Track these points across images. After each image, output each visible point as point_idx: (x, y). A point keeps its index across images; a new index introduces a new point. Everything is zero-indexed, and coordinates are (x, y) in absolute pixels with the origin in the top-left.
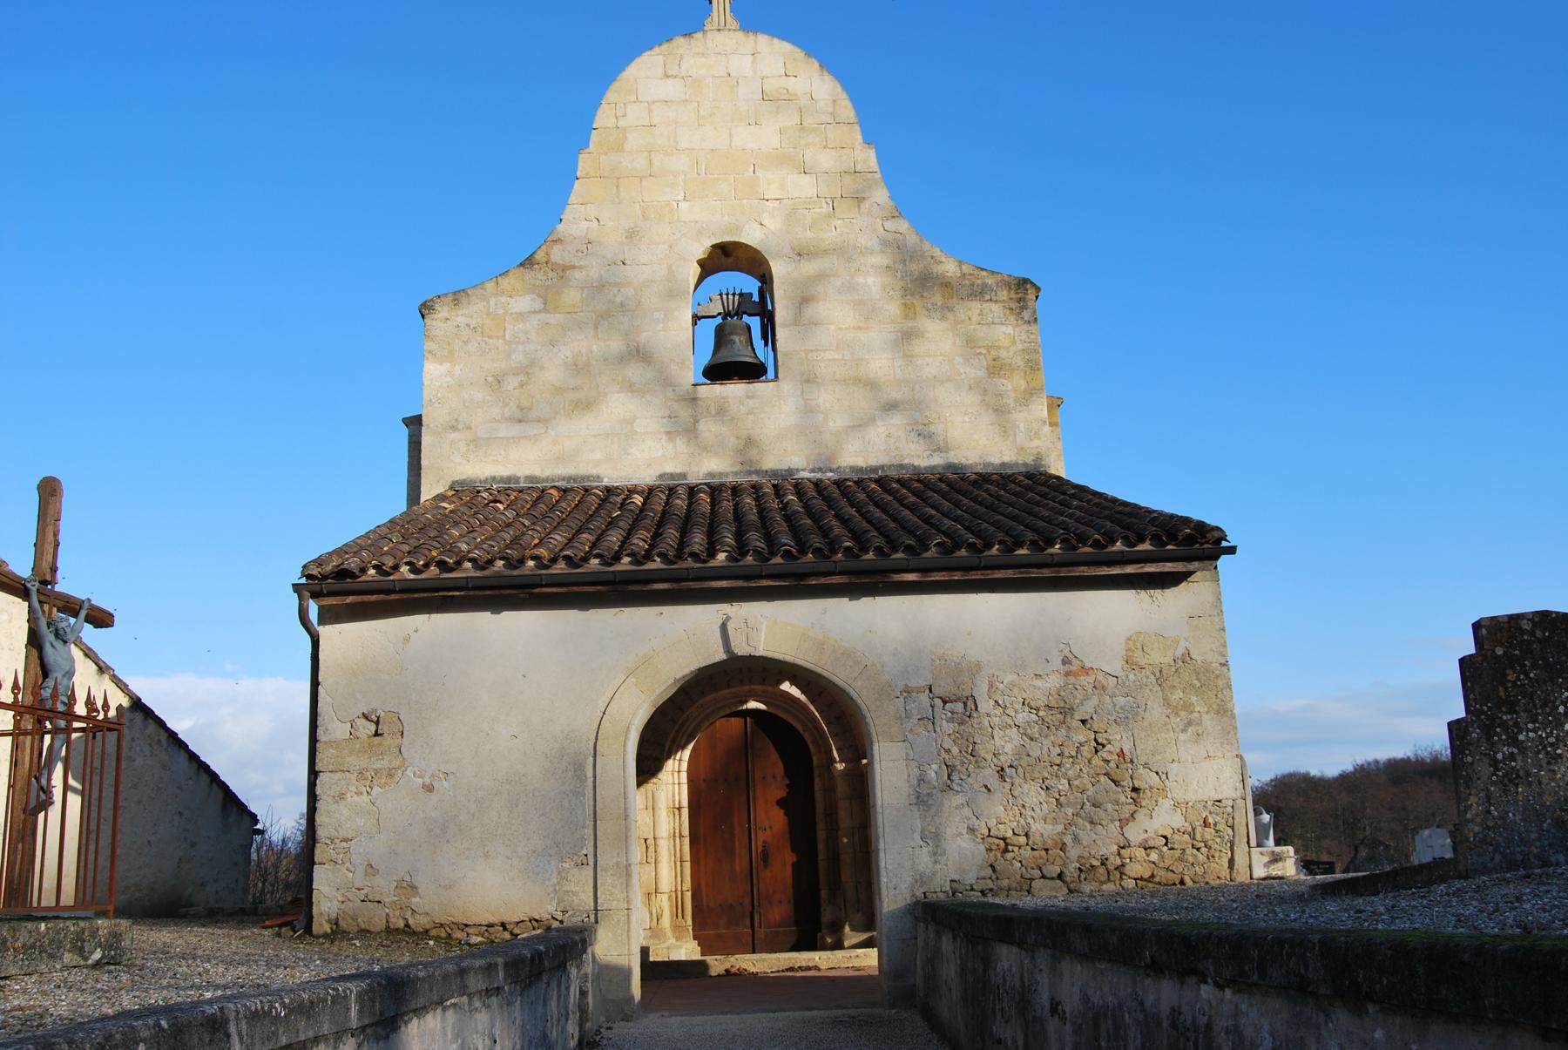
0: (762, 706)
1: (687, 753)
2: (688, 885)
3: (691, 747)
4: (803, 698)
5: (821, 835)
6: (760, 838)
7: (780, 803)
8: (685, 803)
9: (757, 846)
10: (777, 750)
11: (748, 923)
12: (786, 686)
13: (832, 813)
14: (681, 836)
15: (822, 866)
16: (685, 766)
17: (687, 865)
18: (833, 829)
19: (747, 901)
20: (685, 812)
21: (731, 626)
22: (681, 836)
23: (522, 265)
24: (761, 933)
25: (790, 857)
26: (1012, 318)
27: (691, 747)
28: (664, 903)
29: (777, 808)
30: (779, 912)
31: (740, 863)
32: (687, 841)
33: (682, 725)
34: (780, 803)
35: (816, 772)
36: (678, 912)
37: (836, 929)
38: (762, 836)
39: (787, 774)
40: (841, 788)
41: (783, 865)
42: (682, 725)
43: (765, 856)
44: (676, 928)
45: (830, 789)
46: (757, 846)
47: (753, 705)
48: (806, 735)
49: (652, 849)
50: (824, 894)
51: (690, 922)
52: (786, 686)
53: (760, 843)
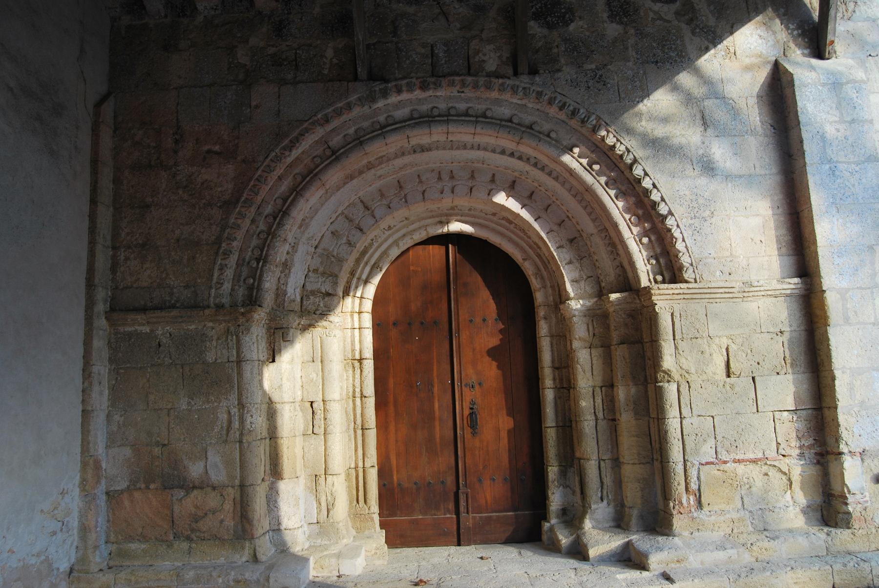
0: (467, 228)
1: (371, 290)
2: (372, 458)
3: (376, 280)
4: (525, 214)
5: (549, 395)
6: (467, 397)
7: (493, 353)
8: (369, 353)
9: (463, 410)
10: (489, 286)
11: (451, 506)
12: (501, 198)
13: (564, 366)
14: (363, 396)
15: (551, 435)
16: (368, 305)
17: (372, 436)
18: (566, 386)
19: (450, 480)
20: (369, 365)
21: (730, 350)
22: (363, 396)
23: (514, 182)
24: (469, 520)
25: (506, 423)
26: (283, 527)
27: (376, 280)
28: (339, 488)
29: (487, 359)
30: (491, 491)
31: (441, 431)
32: (371, 402)
33: (364, 253)
34: (493, 353)
35: (541, 312)
36: (359, 495)
37: (572, 518)
38: (468, 395)
39: (500, 316)
40: (580, 331)
41: (497, 427)
42: (364, 253)
43: (473, 420)
44: (356, 516)
45: (562, 334)
46: (463, 410)
47: (456, 227)
48: (535, 283)
49: (320, 415)
50: (553, 472)
51: (375, 508)
52: (501, 198)
53: (466, 405)
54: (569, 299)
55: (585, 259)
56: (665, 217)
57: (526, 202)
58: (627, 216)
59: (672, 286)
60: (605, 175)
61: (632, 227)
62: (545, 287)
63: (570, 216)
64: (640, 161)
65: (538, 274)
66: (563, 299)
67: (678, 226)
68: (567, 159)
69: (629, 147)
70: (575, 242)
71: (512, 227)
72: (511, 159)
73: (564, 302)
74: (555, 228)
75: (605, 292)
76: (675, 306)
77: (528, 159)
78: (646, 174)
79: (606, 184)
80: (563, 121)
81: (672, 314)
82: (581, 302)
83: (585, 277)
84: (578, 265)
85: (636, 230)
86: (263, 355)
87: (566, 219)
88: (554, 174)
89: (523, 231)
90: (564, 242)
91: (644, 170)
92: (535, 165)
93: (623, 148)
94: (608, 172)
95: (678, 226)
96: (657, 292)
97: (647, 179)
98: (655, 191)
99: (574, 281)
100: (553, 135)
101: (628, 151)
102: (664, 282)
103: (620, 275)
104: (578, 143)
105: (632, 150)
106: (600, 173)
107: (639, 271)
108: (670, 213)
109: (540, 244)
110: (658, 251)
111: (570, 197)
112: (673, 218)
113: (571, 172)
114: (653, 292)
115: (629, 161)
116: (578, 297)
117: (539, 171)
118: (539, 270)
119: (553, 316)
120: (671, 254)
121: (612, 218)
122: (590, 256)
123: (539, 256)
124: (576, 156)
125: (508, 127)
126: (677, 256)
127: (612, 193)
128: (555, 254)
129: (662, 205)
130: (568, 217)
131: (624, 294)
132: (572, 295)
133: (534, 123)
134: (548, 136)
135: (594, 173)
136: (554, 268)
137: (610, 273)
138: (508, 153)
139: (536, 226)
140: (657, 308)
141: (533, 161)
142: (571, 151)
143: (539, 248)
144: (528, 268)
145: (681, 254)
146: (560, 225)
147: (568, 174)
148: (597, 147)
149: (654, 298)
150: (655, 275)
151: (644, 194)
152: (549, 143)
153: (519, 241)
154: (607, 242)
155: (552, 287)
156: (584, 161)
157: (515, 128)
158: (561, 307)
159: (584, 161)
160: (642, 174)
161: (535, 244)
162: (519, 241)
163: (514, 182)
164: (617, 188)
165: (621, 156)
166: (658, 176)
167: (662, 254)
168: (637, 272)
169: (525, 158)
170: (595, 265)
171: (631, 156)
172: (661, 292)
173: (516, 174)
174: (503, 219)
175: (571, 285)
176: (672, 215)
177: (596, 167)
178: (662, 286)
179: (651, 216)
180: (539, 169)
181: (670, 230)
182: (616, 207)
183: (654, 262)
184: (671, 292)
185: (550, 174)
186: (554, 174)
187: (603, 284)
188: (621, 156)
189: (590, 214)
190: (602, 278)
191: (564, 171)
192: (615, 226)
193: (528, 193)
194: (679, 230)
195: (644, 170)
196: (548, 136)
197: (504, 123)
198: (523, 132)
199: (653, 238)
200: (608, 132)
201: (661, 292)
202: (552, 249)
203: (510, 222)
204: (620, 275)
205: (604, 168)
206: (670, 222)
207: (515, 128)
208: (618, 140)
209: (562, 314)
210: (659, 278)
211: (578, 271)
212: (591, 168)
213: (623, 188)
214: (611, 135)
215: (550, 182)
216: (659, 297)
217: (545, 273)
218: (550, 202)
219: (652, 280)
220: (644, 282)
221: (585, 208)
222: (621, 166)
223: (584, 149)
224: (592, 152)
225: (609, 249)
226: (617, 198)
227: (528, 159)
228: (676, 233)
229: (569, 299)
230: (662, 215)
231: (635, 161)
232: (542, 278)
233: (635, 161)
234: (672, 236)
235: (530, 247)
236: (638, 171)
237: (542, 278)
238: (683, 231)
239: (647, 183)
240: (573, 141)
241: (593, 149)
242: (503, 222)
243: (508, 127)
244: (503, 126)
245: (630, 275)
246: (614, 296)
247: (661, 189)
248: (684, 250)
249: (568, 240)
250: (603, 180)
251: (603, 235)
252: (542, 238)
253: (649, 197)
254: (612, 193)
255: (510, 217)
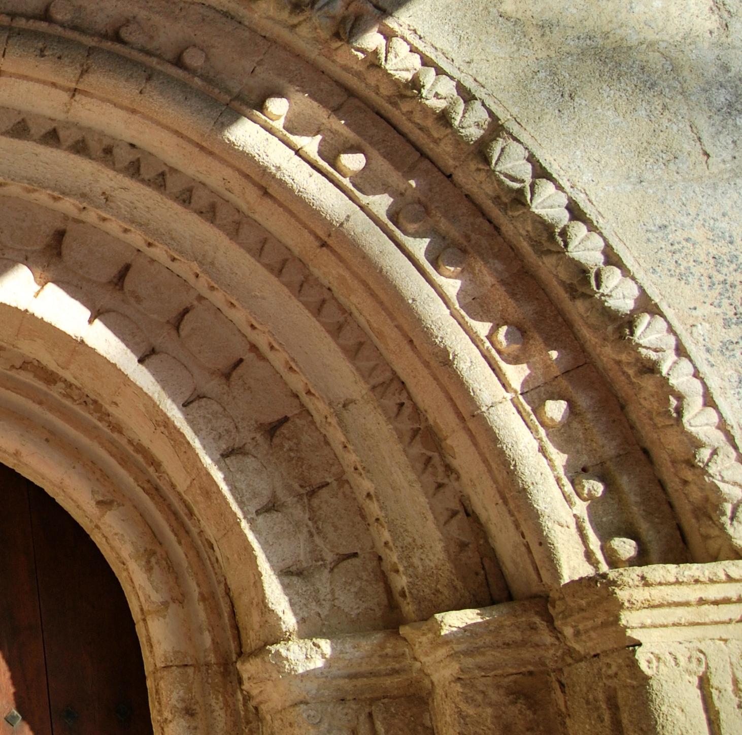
4: (102, 339)
23: (60, 235)
48: (140, 585)
54: (280, 637)
55: (324, 493)
56: (628, 323)
57: (107, 299)
58: (483, 328)
59: (670, 571)
60: (385, 188)
61: (503, 365)
62: (181, 599)
63: (262, 341)
64: (515, 129)
65: (154, 553)
66: (251, 640)
67: (681, 351)
68: (245, 134)
69: (469, 83)
70: (278, 437)
71: (55, 392)
72: (48, 153)
73: (261, 650)
74: (212, 386)
75: (408, 608)
76: (709, 648)
77: (108, 151)
78: (541, 173)
79: (394, 215)
80: (226, 14)
81: (704, 683)
82: (326, 645)
83: (330, 557)
84: (299, 513)
85: (517, 374)
86: (583, 581)
87: (249, 357)
88: (201, 199)
89: (96, 406)
90: (245, 436)
91: (531, 159)
92: (134, 169)
93: (447, 87)
94: (395, 178)
95: (681, 351)
96: (641, 594)
97: (547, 189)
98: (579, 230)
99: (289, 574)
100: (194, 59)
101: (467, 96)
102: (642, 558)
103: (463, 546)
104: (282, 82)
105: (479, 93)
106: (366, 182)
107: (548, 524)
108: (646, 305)
109: (161, 450)
110: (609, 448)
111: (263, 272)
112: (660, 323)
113: (265, 183)
114: (622, 594)
115: (474, 133)
116: (310, 630)
117: (147, 191)
118: (155, 536)
119: (217, 704)
120: (662, 457)
121: (427, 334)
122: (342, 481)
123: (155, 491)
124: (279, 125)
125: (36, 35)
126: (690, 463)
127: (420, 246)
128: (218, 476)
129: (613, 278)
130: (254, 348)
131: (494, 614)
132: (289, 622)
133: (127, 22)
134: (178, 62)
135: (346, 182)
136: (211, 533)
137: (422, 541)
138: (37, 130)
139: (143, 377)
140: (642, 656)
141: (124, 156)
142: (261, 107)
143: (155, 463)
144: (115, 539)
145: (705, 454)
146: (227, 376)
147: (252, 194)
148: (350, 92)
149: (626, 618)
150: (605, 536)
151: (536, 245)
152: (184, 86)
153: (84, 440)
154: (407, 426)
155: (208, 598)
156: (311, 145)
157: (60, 40)
158: (248, 669)
159: (311, 145)
160: (526, 171)
161: (141, 449)
162: (84, 440)
163: (60, 235)
164: (432, 232)
165: (444, 117)
166: (585, 178)
167: (622, 458)
168: (538, 529)
169: (95, 147)
170: (362, 513)
171: (479, 114)
172: (657, 594)
173: (68, 205)
174: (26, 365)
175: (286, 587)
176: (655, 311)
177: (354, 162)
178: (658, 572)
179: (568, 324)
180: (148, 183)
181: (650, 368)
182: (438, 299)
183: (598, 488)
184: (692, 593)
185: (186, 198)
186: (201, 199)
187: (401, 582)
188: (444, 117)
189: (336, 331)
190: (393, 557)
191: (236, 182)
192: (442, 362)
193: (112, 272)
194: (685, 364)
195: (531, 159)
196: (178, 62)
197: (22, 23)
198: (90, 51)
199: (583, 402)
200: (389, 36)
201: (657, 594)
202: (207, 460)
203: (50, 378)
204: (463, 546)
205: (382, 165)
206: (649, 335)
207: (60, 40)
208: (426, 62)
209: (247, 698)
210: (626, 547)
211: (303, 536)
212: (333, 165)
213: (454, 233)
214: (399, 46)
215: (188, 225)
216: (647, 616)
217: (179, 552)
218: (188, 299)
219: (599, 556)
220: (572, 565)
221: (318, 310)
222: (444, 151)
223: (303, 101)
224: (336, 110)
225: (417, 449)
226: (435, 264)
227: (108, 151)
228: (680, 377)
229: (280, 637)
230: (610, 315)
231: (496, 129)
232: (171, 568)
233: (496, 129)
234: (665, 388)
235: (124, 461)
236: (511, 163)
237: (171, 568)
238: (704, 369)
239: (548, 204)
240: (265, 76)
241: (336, 101)
242: (26, 377)
243: (36, 35)
244: (21, 32)
245: (505, 540)
246: (456, 620)
247: (601, 223)
248: (718, 438)
249: (260, 427)
250: (381, 203)
251: (391, 402)
252: (166, 423)
253: (561, 252)
254: (420, 246)
255: (49, 361)
